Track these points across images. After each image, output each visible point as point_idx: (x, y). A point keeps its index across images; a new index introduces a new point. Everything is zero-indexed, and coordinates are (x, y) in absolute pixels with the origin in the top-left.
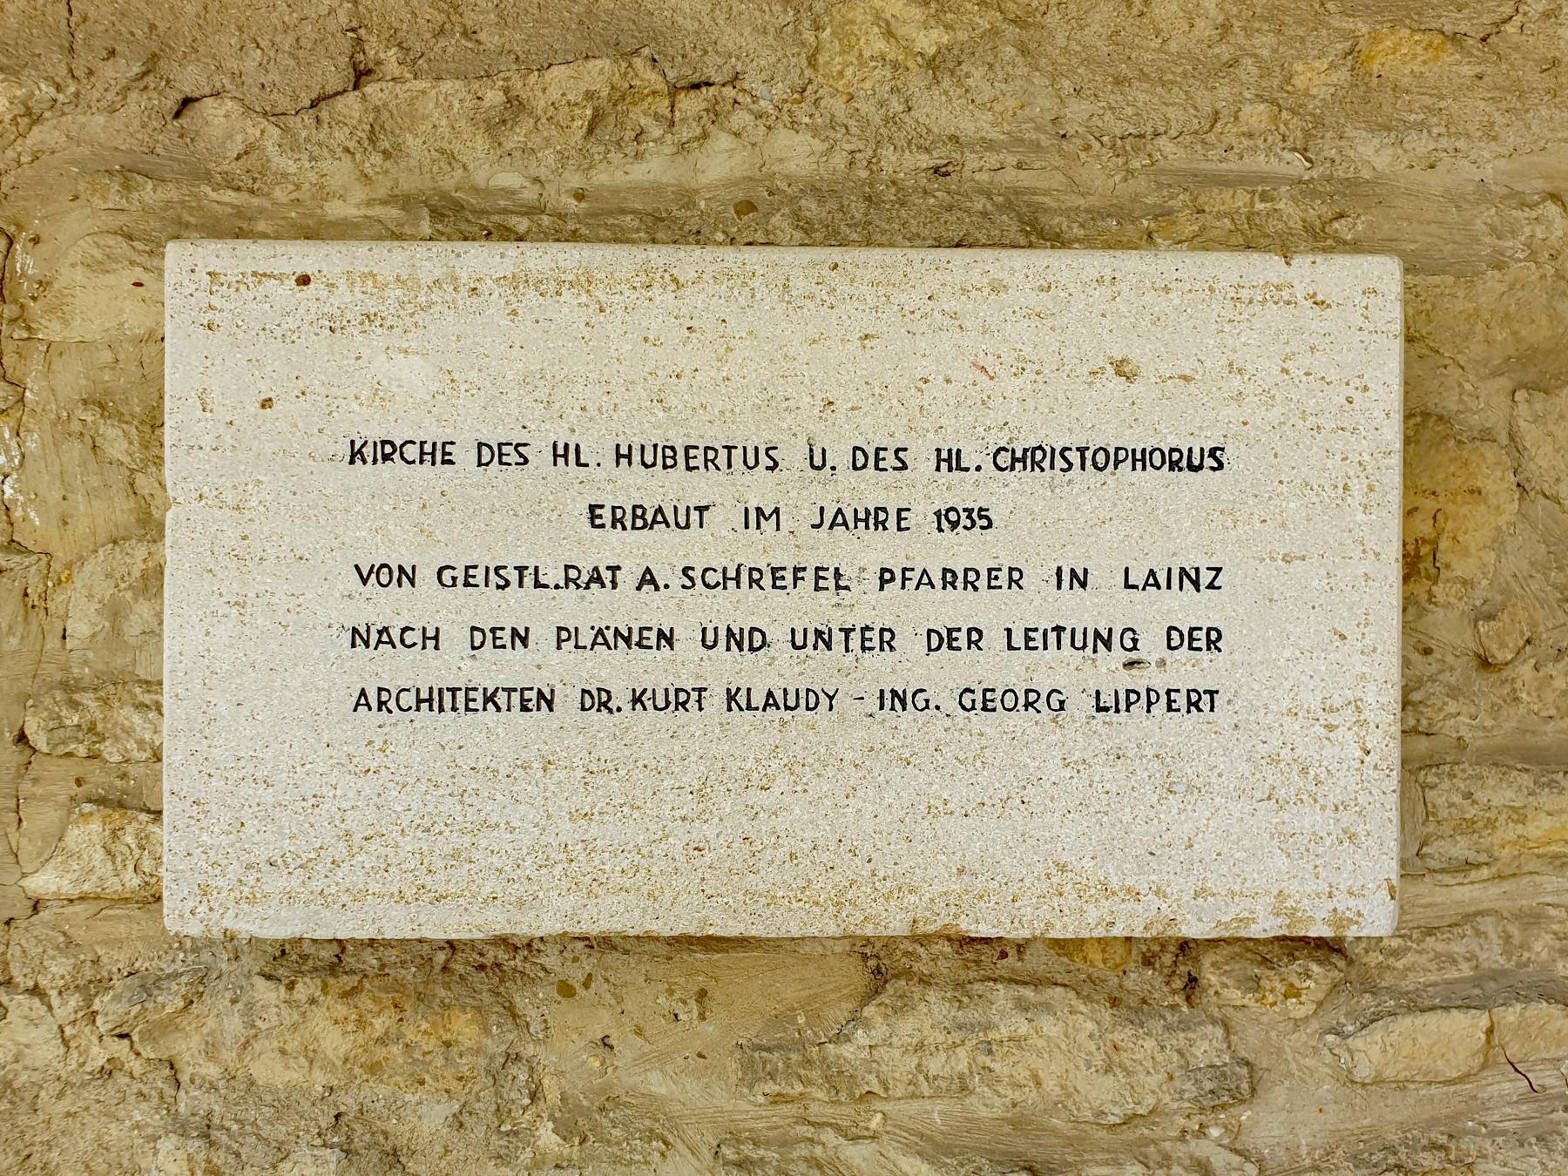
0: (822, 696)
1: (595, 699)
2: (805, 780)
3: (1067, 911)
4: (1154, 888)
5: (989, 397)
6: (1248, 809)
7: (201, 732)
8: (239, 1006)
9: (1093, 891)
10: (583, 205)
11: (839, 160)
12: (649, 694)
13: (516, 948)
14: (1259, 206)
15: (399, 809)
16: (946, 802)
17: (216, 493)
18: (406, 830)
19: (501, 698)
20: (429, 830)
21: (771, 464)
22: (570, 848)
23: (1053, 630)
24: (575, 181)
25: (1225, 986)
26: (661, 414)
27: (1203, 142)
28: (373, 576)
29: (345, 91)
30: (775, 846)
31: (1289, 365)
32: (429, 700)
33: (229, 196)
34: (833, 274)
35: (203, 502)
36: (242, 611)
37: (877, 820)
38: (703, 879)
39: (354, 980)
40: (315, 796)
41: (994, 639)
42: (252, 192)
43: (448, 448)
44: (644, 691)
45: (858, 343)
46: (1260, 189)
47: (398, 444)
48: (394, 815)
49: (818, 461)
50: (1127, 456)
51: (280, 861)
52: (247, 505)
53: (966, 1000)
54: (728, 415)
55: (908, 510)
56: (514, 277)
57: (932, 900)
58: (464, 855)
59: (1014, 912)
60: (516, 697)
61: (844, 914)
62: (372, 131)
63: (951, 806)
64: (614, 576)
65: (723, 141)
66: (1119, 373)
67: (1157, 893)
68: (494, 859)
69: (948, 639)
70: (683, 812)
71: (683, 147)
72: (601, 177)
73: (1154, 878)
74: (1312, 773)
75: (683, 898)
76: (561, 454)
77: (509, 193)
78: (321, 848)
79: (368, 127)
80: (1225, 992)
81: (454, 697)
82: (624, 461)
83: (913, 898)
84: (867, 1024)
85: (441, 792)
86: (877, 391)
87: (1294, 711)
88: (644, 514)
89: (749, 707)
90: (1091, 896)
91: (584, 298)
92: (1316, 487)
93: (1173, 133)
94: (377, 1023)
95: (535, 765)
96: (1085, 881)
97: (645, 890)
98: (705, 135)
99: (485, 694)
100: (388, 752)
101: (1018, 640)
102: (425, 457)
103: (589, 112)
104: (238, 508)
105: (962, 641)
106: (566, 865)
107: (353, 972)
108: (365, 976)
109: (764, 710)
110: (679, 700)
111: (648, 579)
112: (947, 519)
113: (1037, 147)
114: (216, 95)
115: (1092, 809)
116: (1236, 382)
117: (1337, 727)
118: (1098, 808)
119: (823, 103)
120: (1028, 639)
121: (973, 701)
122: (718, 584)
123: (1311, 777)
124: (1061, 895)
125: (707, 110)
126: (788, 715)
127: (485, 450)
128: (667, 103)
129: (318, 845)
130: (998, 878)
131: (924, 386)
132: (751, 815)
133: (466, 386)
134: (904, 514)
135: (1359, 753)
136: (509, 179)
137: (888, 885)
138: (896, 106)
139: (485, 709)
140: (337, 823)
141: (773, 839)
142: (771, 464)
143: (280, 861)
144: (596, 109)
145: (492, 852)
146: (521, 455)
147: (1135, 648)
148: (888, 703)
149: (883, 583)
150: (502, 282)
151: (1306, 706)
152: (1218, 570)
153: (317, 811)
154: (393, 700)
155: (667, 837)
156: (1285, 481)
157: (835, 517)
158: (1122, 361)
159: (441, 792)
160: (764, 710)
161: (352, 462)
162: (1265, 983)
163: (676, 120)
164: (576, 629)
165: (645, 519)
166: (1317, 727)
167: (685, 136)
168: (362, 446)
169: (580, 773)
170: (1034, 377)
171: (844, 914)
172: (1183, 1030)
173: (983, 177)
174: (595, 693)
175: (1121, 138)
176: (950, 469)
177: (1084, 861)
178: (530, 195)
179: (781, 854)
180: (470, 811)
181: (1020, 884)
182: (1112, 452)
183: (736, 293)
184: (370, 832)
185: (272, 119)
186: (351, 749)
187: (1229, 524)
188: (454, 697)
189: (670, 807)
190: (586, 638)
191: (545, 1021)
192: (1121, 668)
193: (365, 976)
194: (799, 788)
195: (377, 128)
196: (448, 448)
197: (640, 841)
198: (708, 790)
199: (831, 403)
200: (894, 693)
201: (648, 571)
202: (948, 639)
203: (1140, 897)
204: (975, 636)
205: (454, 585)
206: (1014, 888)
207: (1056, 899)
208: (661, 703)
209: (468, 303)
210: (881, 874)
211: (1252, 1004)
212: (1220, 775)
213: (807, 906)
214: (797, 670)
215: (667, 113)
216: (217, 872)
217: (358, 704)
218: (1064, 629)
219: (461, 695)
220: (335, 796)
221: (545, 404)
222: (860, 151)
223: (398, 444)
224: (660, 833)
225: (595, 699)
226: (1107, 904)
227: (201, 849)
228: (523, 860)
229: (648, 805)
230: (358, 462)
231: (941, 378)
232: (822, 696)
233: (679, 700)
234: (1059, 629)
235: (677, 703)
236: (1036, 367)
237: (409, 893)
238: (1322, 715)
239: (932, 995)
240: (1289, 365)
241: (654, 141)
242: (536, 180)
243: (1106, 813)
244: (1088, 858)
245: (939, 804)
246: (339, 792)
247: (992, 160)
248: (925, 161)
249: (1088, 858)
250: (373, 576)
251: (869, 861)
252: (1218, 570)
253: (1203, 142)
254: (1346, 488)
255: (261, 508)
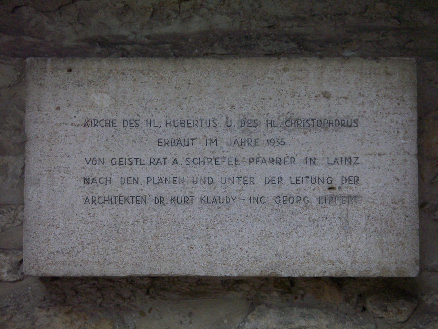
0: (231, 199)
1: (160, 200)
2: (226, 226)
3: (311, 268)
4: (339, 260)
5: (284, 104)
6: (369, 235)
7: (36, 211)
8: (29, 318)
9: (319, 261)
10: (150, 41)
11: (237, 25)
12: (176, 198)
13: (125, 299)
14: (381, 38)
15: (99, 235)
16: (271, 233)
17: (42, 136)
18: (101, 241)
19: (130, 200)
20: (107, 241)
21: (215, 125)
22: (152, 247)
23: (305, 177)
24: (146, 32)
25: (375, 309)
26: (180, 110)
27: (363, 16)
28: (91, 162)
29: (69, 3)
30: (217, 247)
31: (379, 93)
32: (109, 200)
33: (31, 39)
34: (234, 66)
35: (38, 139)
36: (50, 173)
37: (249, 239)
38: (193, 258)
39: (70, 308)
40: (72, 231)
41: (286, 181)
42: (38, 38)
43: (114, 122)
44: (175, 197)
45: (241, 87)
46: (381, 32)
47: (99, 120)
48: (97, 237)
49: (229, 124)
50: (327, 122)
51: (61, 251)
52: (52, 140)
53: (283, 313)
54: (201, 110)
55: (258, 139)
56: (135, 69)
57: (267, 264)
58: (118, 249)
59: (294, 268)
60: (134, 199)
61: (239, 269)
62: (78, 17)
63: (273, 234)
64: (165, 160)
65: (197, 18)
66: (324, 96)
67: (340, 262)
68: (128, 251)
69: (271, 181)
70: (187, 236)
71: (184, 21)
72: (156, 31)
73: (338, 257)
74: (389, 223)
75: (188, 263)
76: (149, 123)
77: (124, 37)
78: (74, 247)
79: (77, 16)
80: (374, 311)
81: (115, 199)
82: (168, 125)
83: (261, 264)
84: (248, 321)
85: (111, 229)
86: (248, 102)
87: (383, 203)
88: (175, 141)
89: (207, 203)
90: (318, 263)
91: (156, 75)
92: (388, 132)
93: (352, 13)
94: (77, 323)
95: (141, 221)
96: (316, 258)
97: (175, 261)
98: (191, 17)
99: (125, 198)
100: (95, 217)
101: (294, 180)
102: (107, 125)
103: (152, 10)
104: (49, 141)
105: (276, 181)
106: (150, 253)
107: (69, 305)
108: (74, 307)
109: (212, 203)
110: (186, 200)
111: (175, 162)
112: (270, 142)
113: (304, 19)
114: (26, 5)
115: (318, 235)
116: (362, 99)
117: (397, 208)
118: (320, 235)
119: (231, 5)
120: (297, 181)
121: (280, 200)
122: (198, 163)
123: (389, 224)
124: (309, 263)
125: (191, 8)
126: (220, 205)
127: (126, 122)
128: (178, 6)
129: (73, 246)
130: (288, 257)
131: (263, 101)
132: (209, 237)
133: (120, 102)
134: (257, 141)
135: (404, 217)
136: (124, 32)
137: (253, 260)
138: (256, 6)
139: (125, 203)
140: (79, 239)
141: (216, 245)
142: (215, 125)
143: (61, 251)
144: (154, 9)
145: (127, 248)
146: (137, 124)
147: (331, 183)
148: (252, 201)
149: (250, 162)
150: (131, 70)
151: (386, 202)
152: (357, 158)
153: (72, 235)
154: (97, 200)
155: (182, 244)
156: (378, 130)
157: (235, 142)
158: (325, 93)
159: (111, 229)
160: (212, 203)
161: (85, 126)
162: (389, 309)
163: (181, 12)
164: (153, 178)
165: (178, 143)
166: (390, 208)
167: (184, 17)
168: (88, 121)
169: (155, 223)
170: (297, 98)
171: (239, 269)
172: (360, 325)
173: (286, 29)
174: (159, 198)
175: (334, 15)
176: (272, 126)
177: (316, 252)
178: (132, 38)
179: (219, 249)
180: (121, 235)
181: (295, 259)
182: (323, 121)
183: (204, 73)
184: (89, 242)
185: (46, 13)
186: (84, 216)
187: (361, 144)
188: (115, 199)
189: (183, 234)
190: (156, 181)
191: (135, 325)
192: (327, 190)
193: (74, 307)
194: (224, 228)
195: (80, 16)
196: (114, 122)
197: (173, 245)
198: (195, 229)
199: (233, 106)
200: (254, 198)
201: (176, 159)
202: (271, 181)
203: (334, 263)
204: (280, 179)
205: (116, 164)
206: (294, 260)
207: (307, 264)
208: (180, 201)
209: (121, 77)
210: (251, 256)
211: (385, 316)
212: (359, 224)
213: (227, 266)
214: (223, 191)
215: (178, 9)
216: (41, 255)
217: (86, 202)
218: (309, 177)
219: (117, 199)
220: (78, 231)
221: (144, 108)
222: (244, 21)
223: (99, 120)
224: (180, 243)
225: (160, 200)
226: (323, 265)
227: (36, 248)
228: (137, 251)
229: (176, 234)
230: (87, 126)
231: (268, 98)
232: (231, 199)
233: (186, 200)
234: (307, 177)
235: (185, 201)
236: (298, 94)
237: (102, 261)
238: (392, 205)
239: (271, 311)
240: (379, 93)
241: (174, 19)
242: (134, 33)
243: (323, 236)
244: (317, 251)
245: (269, 233)
246: (80, 229)
247: (289, 24)
248: (266, 24)
249: (317, 251)
250: (91, 162)
251: (247, 252)
252: (357, 158)
253: (363, 16)
254: (398, 132)
255: (56, 141)
